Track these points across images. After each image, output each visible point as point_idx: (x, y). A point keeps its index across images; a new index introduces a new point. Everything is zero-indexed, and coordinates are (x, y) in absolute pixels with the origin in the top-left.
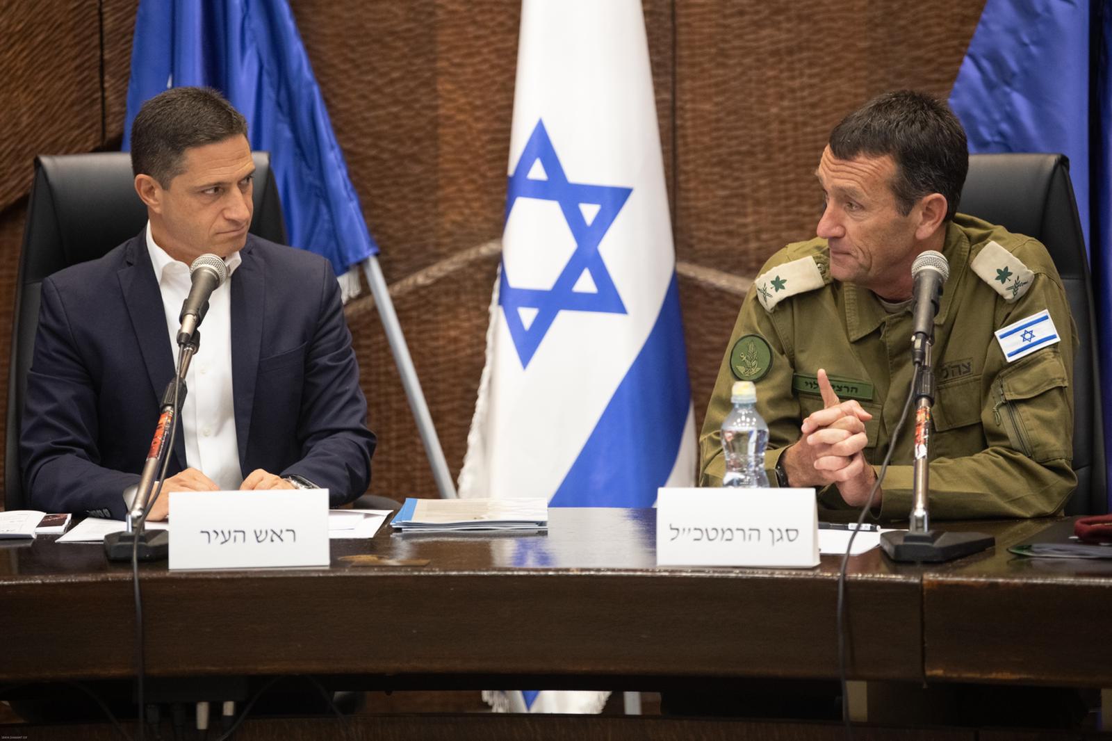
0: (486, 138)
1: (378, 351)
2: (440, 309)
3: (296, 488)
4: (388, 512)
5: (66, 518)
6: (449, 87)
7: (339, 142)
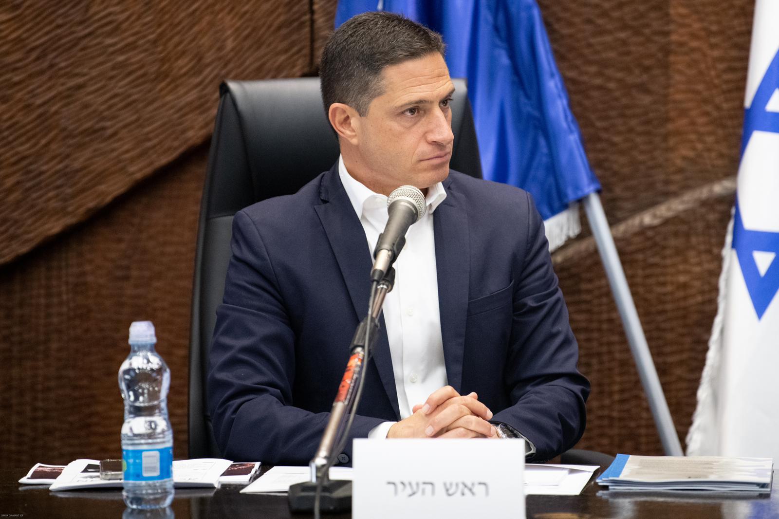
0: (721, 66)
1: (600, 296)
2: (668, 252)
3: (484, 436)
4: (595, 468)
5: (253, 467)
6: (683, 11)
7: (560, 69)
